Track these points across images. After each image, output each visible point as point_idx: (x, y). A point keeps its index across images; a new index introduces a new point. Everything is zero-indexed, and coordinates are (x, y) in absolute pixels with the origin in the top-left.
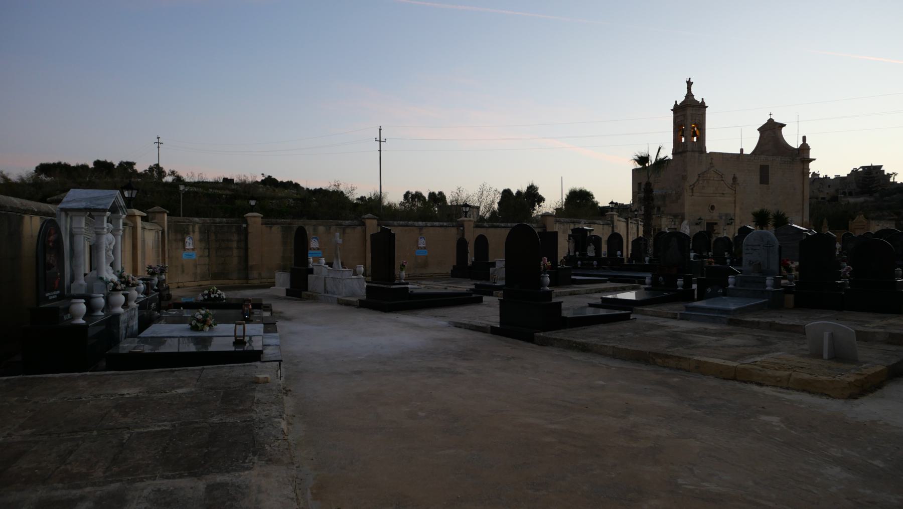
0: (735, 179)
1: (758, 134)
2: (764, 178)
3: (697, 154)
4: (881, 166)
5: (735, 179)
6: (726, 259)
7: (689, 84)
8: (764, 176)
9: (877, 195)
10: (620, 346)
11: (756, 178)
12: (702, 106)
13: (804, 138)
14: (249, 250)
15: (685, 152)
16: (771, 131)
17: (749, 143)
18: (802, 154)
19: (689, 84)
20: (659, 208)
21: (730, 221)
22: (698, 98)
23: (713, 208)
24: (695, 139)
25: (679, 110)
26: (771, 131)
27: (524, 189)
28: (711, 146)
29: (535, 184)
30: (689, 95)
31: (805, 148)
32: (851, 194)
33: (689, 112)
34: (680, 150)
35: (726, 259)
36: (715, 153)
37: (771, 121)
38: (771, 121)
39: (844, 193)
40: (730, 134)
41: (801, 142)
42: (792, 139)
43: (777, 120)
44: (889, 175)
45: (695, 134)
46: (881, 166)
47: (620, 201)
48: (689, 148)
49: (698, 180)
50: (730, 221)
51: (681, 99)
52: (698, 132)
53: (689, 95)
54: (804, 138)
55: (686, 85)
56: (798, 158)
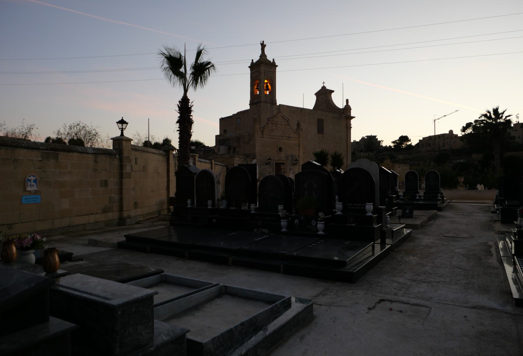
0: (298, 125)
1: (315, 98)
2: (320, 130)
3: (269, 105)
4: (376, 136)
5: (298, 125)
6: (279, 219)
7: (263, 46)
8: (320, 125)
9: (375, 152)
10: (197, 279)
11: (314, 129)
12: (273, 65)
13: (347, 101)
14: (170, 182)
15: (259, 102)
16: (324, 95)
17: (309, 103)
18: (345, 115)
19: (263, 46)
20: (234, 149)
21: (295, 162)
22: (270, 58)
23: (280, 149)
24: (268, 93)
25: (254, 67)
26: (324, 95)
27: (161, 141)
28: (280, 101)
29: (169, 138)
30: (263, 55)
31: (348, 108)
32: (361, 151)
33: (263, 68)
34: (256, 101)
35: (279, 219)
36: (284, 106)
37: (324, 88)
38: (324, 88)
39: (358, 150)
40: (294, 92)
41: (345, 104)
42: (339, 102)
43: (328, 87)
44: (380, 142)
45: (267, 89)
46: (376, 136)
47: (192, 137)
48: (263, 99)
49: (267, 123)
50: (295, 162)
51: (256, 58)
52: (270, 87)
53: (263, 55)
54: (347, 101)
55: (260, 47)
56: (344, 115)
